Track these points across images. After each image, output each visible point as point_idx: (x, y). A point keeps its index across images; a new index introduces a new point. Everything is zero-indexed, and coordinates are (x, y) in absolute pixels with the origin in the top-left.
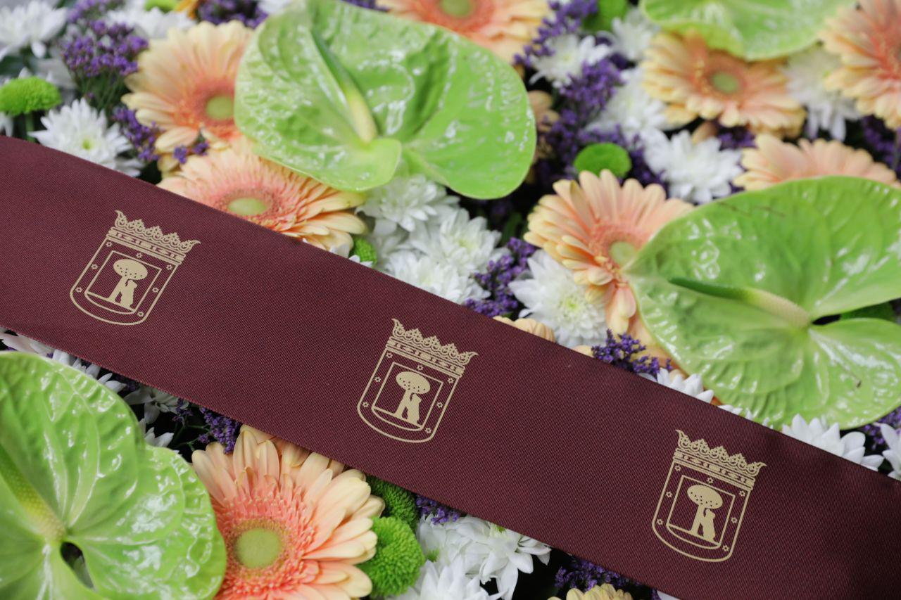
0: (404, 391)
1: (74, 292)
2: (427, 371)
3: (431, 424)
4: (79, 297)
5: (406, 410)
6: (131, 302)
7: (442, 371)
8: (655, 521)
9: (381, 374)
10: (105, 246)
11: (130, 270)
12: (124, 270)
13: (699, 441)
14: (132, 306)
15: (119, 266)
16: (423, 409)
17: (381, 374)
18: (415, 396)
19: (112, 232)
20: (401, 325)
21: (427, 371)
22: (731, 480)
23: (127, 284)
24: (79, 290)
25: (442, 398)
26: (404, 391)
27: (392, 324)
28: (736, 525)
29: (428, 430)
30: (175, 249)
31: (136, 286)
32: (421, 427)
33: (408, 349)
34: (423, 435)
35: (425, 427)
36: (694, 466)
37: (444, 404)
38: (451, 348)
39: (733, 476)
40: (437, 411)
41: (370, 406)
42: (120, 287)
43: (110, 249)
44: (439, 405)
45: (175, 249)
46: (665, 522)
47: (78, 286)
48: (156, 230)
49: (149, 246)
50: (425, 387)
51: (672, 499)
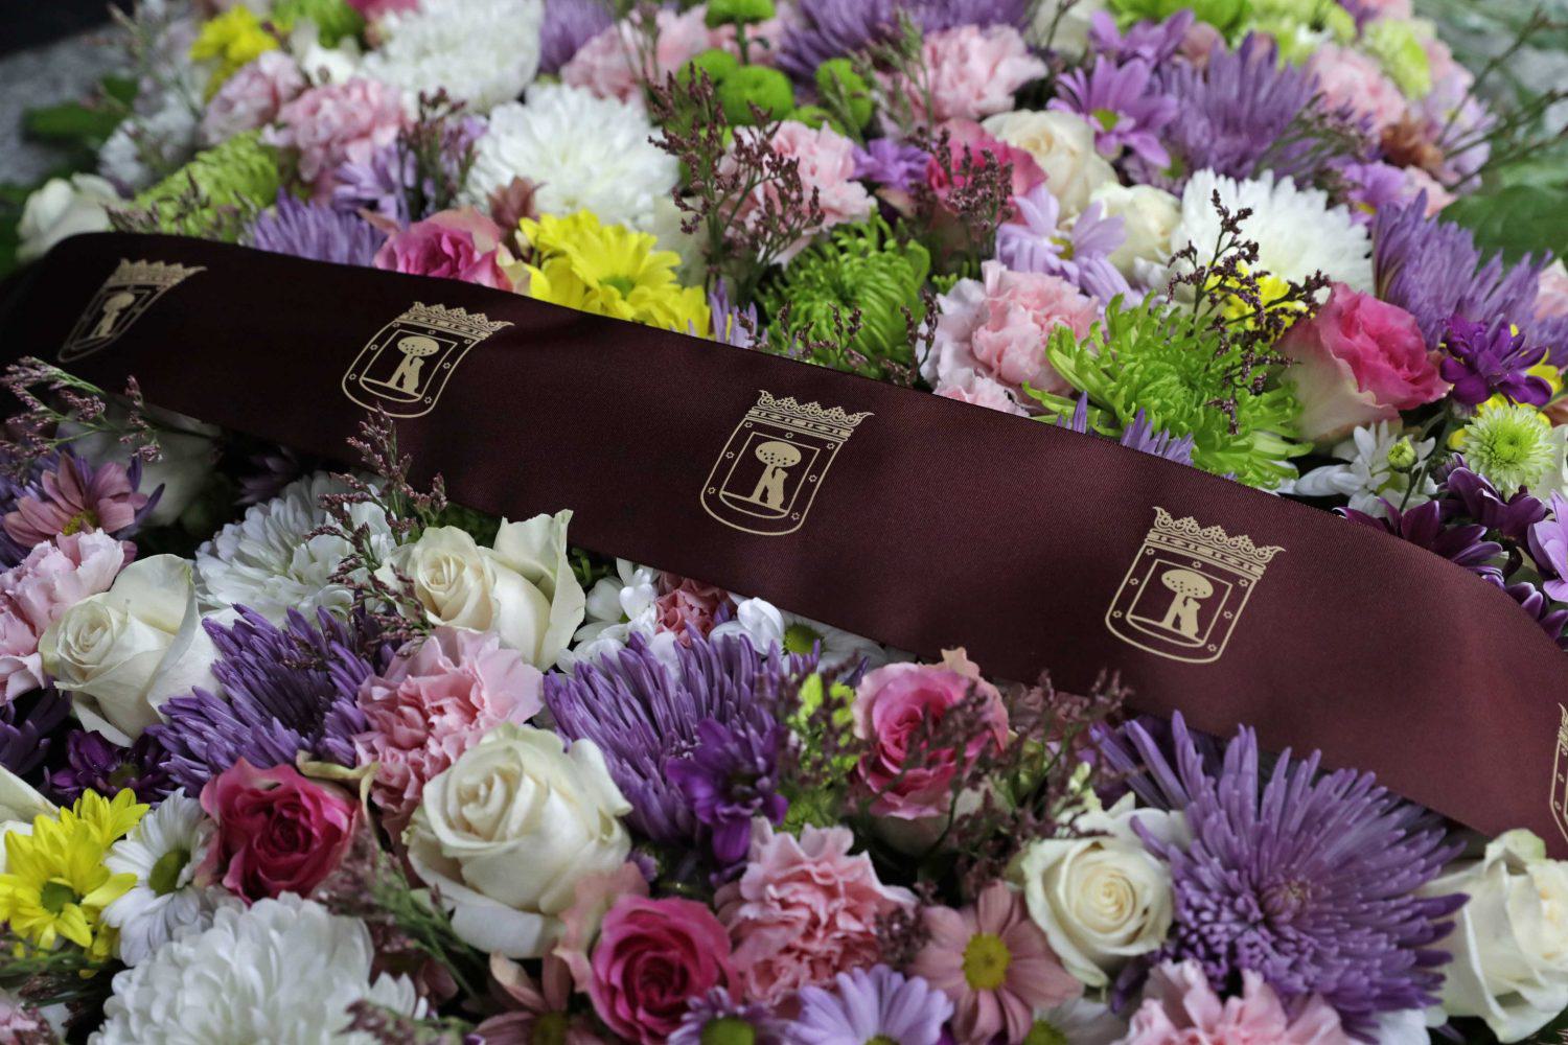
0: (765, 466)
1: (706, 494)
2: (1206, 568)
3: (1216, 639)
4: (1117, 623)
5: (766, 491)
6: (416, 385)
7: (1229, 569)
8: (349, 375)
9: (1140, 573)
10: (1144, 554)
11: (780, 454)
12: (1178, 583)
13: (1186, 520)
14: (1197, 635)
15: (764, 451)
16: (1203, 618)
17: (1140, 573)
18: (1190, 601)
19: (1152, 536)
20: (1166, 514)
21: (1206, 568)
22: (1231, 565)
23: (774, 474)
24: (1118, 614)
25: (1232, 606)
26: (765, 466)
27: (1155, 514)
28: (1230, 621)
29: (1212, 648)
30: (1252, 560)
31: (785, 475)
32: (420, 397)
33: (823, 428)
34: (1203, 652)
35: (1208, 643)
36: (1177, 547)
37: (1234, 613)
38: (1244, 541)
39: (1178, 542)
40: (1223, 624)
41: (717, 492)
42: (766, 480)
43: (1152, 558)
44: (1228, 615)
45: (1252, 560)
46: (1125, 614)
47: (1115, 609)
48: (1217, 531)
49: (1209, 552)
50: (1206, 590)
51: (1137, 588)
